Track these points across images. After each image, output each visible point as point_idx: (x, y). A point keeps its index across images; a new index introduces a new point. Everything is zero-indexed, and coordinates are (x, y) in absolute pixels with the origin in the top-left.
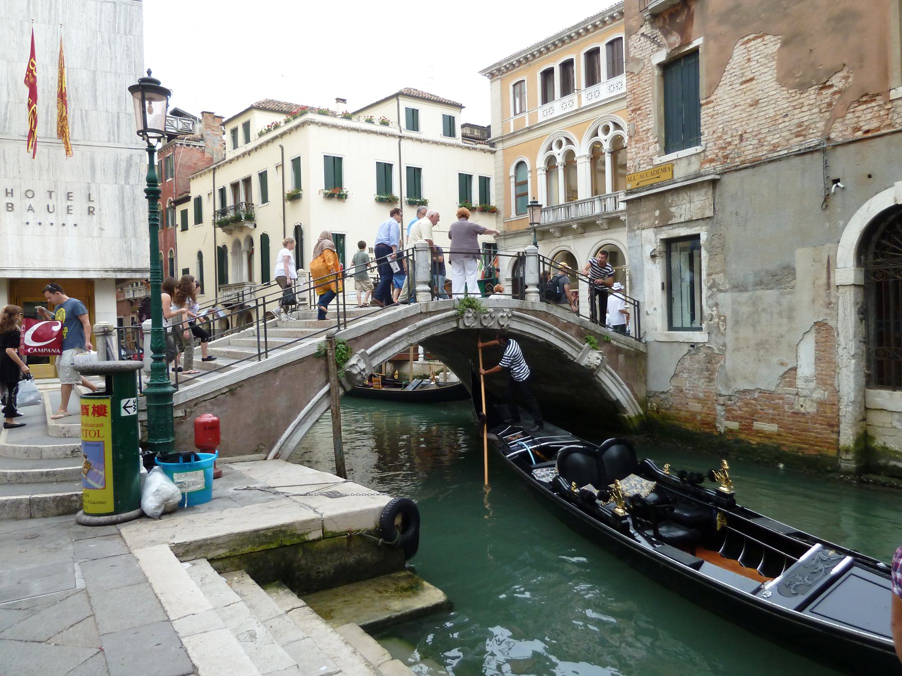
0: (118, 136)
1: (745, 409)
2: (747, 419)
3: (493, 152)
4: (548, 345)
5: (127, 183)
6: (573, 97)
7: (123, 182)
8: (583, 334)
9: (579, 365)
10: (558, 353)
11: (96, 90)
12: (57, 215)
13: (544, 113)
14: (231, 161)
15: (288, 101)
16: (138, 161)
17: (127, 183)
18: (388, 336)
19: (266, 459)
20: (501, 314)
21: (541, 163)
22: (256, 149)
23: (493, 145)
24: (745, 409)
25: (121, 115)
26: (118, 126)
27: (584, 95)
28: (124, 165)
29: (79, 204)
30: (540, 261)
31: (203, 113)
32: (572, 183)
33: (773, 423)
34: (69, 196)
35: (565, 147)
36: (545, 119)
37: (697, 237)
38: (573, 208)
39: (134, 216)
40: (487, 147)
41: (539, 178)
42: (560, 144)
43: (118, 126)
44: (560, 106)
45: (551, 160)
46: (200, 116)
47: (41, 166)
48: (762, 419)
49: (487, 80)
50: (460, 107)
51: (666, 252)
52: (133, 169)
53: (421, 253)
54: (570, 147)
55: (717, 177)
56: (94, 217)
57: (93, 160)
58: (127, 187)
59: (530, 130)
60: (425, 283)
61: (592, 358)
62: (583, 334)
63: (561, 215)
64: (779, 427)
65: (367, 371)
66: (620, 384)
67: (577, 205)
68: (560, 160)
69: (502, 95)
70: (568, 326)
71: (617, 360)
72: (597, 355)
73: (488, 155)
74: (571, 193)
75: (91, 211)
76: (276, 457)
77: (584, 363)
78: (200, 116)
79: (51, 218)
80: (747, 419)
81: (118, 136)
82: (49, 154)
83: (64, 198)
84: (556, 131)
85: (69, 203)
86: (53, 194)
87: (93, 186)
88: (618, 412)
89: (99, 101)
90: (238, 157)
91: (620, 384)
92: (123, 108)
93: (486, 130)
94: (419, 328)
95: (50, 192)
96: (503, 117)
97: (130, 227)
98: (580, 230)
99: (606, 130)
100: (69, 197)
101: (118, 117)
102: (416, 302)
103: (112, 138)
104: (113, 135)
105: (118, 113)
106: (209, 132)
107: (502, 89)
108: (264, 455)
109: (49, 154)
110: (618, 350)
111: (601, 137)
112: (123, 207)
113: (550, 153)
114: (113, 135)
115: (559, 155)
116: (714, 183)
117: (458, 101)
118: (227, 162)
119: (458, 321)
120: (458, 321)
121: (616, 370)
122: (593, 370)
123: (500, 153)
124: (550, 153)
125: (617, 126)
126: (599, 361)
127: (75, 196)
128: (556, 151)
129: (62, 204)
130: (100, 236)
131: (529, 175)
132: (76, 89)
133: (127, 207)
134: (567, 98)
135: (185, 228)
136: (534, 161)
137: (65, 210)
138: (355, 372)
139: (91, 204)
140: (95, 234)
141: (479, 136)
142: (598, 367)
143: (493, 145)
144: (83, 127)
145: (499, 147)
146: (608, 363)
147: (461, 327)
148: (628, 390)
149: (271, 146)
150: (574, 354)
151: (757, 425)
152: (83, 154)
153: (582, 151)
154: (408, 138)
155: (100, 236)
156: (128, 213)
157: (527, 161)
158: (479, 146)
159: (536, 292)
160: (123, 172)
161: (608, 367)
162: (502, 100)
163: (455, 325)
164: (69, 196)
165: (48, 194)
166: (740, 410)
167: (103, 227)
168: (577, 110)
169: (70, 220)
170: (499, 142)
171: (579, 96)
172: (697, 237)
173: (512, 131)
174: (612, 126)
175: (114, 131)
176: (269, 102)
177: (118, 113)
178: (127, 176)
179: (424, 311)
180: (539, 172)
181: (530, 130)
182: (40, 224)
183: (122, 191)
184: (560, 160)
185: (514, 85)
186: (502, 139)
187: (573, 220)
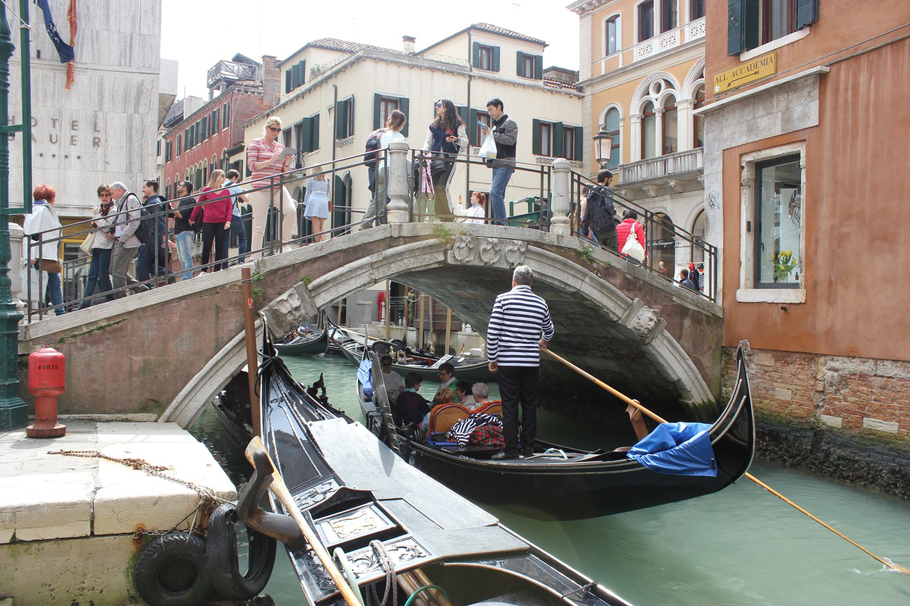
0: (130, 59)
1: (852, 399)
2: (855, 413)
3: (581, 98)
4: (578, 296)
5: (136, 111)
6: (675, 33)
7: (131, 111)
8: (634, 285)
9: (626, 327)
10: (594, 312)
11: (108, 8)
12: (60, 146)
13: (640, 52)
14: (284, 105)
15: (351, 40)
16: (150, 87)
17: (136, 111)
18: (342, 265)
19: (156, 421)
20: (510, 247)
21: (635, 110)
22: (310, 90)
23: (580, 89)
24: (852, 399)
25: (135, 36)
26: (131, 48)
27: (687, 30)
28: (134, 91)
29: (84, 135)
30: (573, 180)
31: (264, 57)
32: (671, 134)
33: (892, 420)
34: (74, 125)
35: (664, 91)
36: (642, 58)
37: (797, 156)
38: (671, 162)
39: (142, 148)
40: (574, 92)
41: (633, 127)
42: (658, 88)
43: (131, 48)
44: (658, 43)
45: (647, 108)
46: (261, 62)
47: (45, 91)
48: (878, 412)
49: (576, 17)
50: (544, 45)
51: (755, 181)
52: (143, 96)
53: (395, 156)
54: (671, 90)
55: (827, 69)
56: (100, 149)
57: (101, 85)
58: (137, 115)
59: (624, 71)
60: (401, 197)
61: (643, 318)
62: (634, 285)
63: (658, 170)
64: (900, 427)
65: (303, 311)
66: (683, 358)
67: (675, 159)
68: (658, 106)
69: (593, 32)
70: (608, 272)
71: (682, 325)
72: (650, 315)
73: (575, 100)
74: (668, 147)
75: (96, 143)
76: (168, 421)
77: (632, 324)
78: (261, 62)
79: (54, 149)
80: (855, 413)
81: (130, 59)
82: (55, 79)
83: (68, 127)
84: (655, 73)
85: (73, 133)
86: (57, 123)
87: (100, 114)
88: (680, 396)
89: (112, 21)
90: (291, 101)
91: (683, 358)
92: (137, 28)
93: (573, 75)
94: (385, 259)
95: (54, 121)
96: (593, 57)
97: (136, 161)
98: (679, 189)
99: (658, 88)
100: (73, 126)
101: (131, 38)
102: (386, 223)
103: (123, 62)
104: (125, 58)
105: (132, 35)
106: (269, 77)
107: (593, 26)
108: (154, 416)
109: (55, 79)
110: (683, 312)
111: (653, 96)
112: (130, 138)
113: (646, 98)
114: (125, 58)
115: (657, 100)
116: (822, 77)
117: (541, 38)
118: (280, 107)
119: (445, 253)
120: (445, 253)
121: (678, 340)
122: (643, 337)
123: (588, 99)
124: (646, 98)
125: (669, 84)
126: (652, 323)
127: (81, 125)
128: (653, 96)
129: (67, 133)
130: (105, 171)
131: (621, 124)
132: (88, 8)
133: (135, 138)
134: (668, 35)
135: (205, 169)
136: (627, 106)
137: (69, 141)
138: (284, 310)
139: (97, 135)
140: (99, 168)
141: (566, 81)
142: (650, 331)
143: (580, 89)
144: (93, 49)
145: (588, 92)
146: (666, 328)
147: (450, 261)
148: (693, 366)
149: (324, 86)
150: (619, 312)
151: (870, 423)
152: (91, 79)
153: (684, 94)
154: (480, 77)
155: (105, 171)
156: (136, 145)
157: (619, 108)
158: (564, 90)
159: (565, 222)
160: (133, 99)
161: (667, 333)
162: (593, 38)
163: (441, 258)
164: (74, 125)
165: (51, 123)
166: (846, 400)
167: (108, 160)
168: (678, 47)
169: (74, 152)
170: (588, 86)
171: (682, 32)
172: (797, 156)
173: (603, 73)
174: (663, 84)
175: (125, 54)
176: (328, 40)
177: (132, 35)
178: (137, 105)
179: (395, 235)
180: (633, 120)
181: (624, 71)
182: (41, 155)
183: (130, 120)
184: (658, 106)
185: (608, 21)
186: (591, 82)
187: (670, 176)
